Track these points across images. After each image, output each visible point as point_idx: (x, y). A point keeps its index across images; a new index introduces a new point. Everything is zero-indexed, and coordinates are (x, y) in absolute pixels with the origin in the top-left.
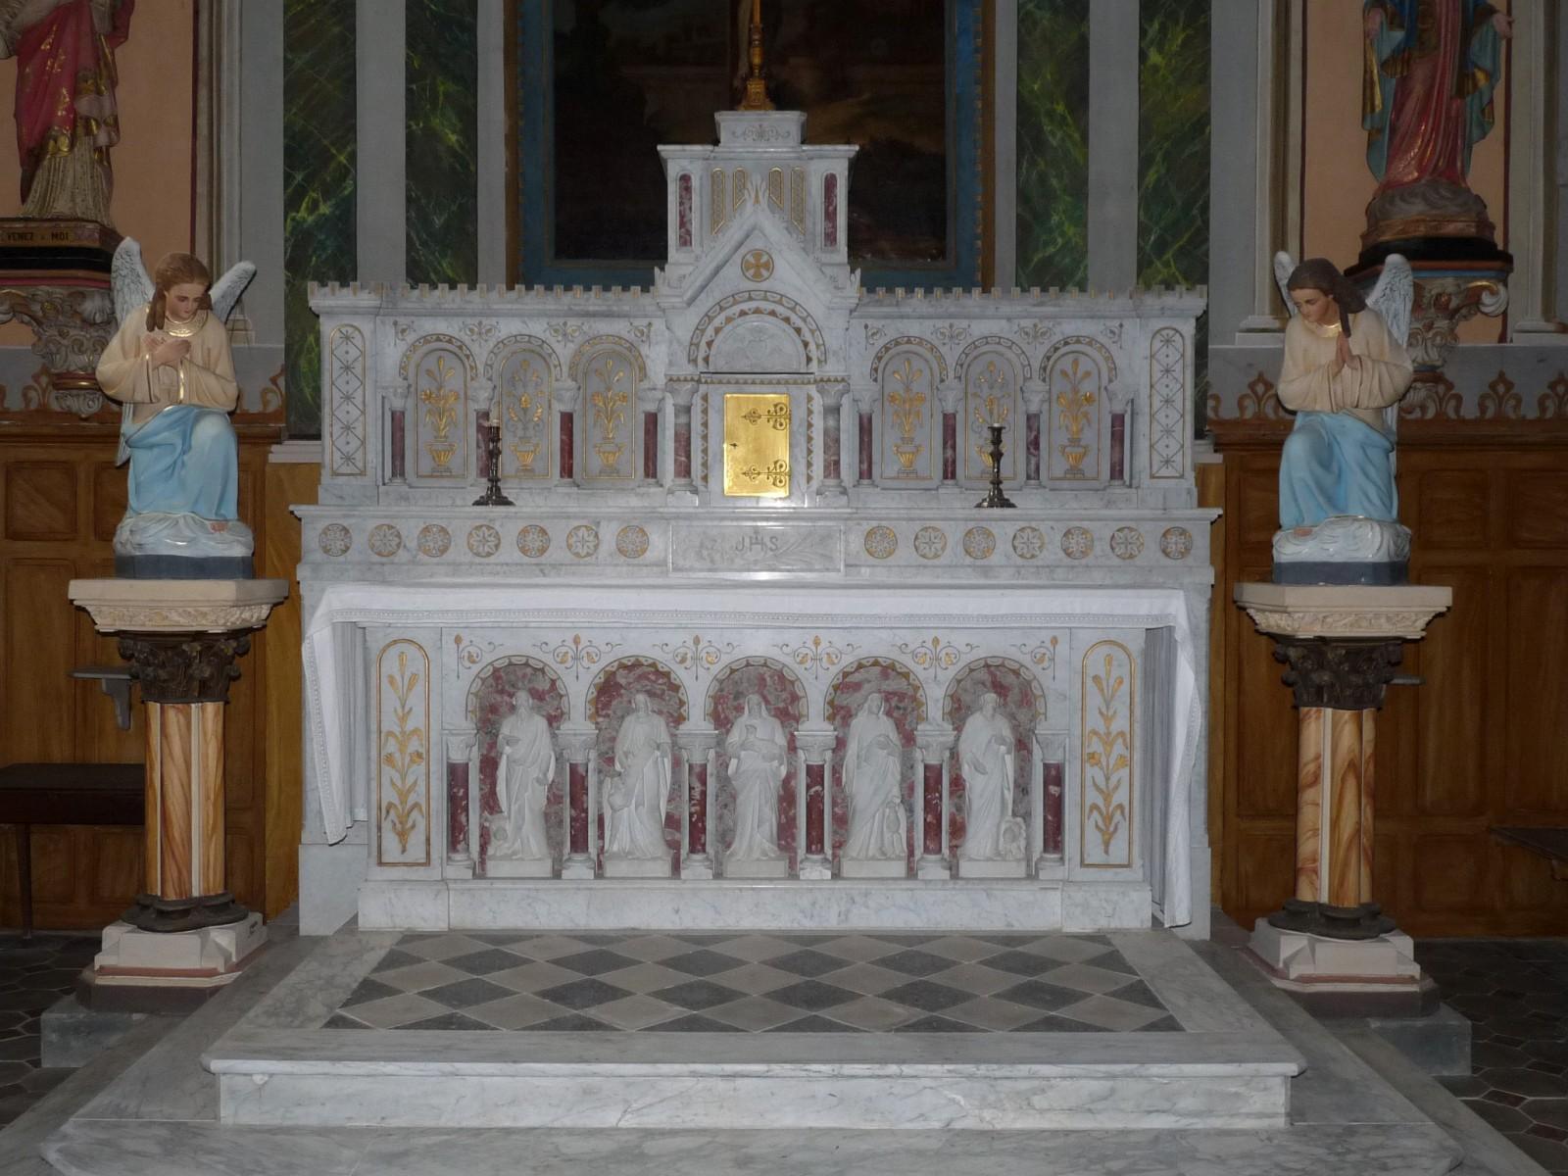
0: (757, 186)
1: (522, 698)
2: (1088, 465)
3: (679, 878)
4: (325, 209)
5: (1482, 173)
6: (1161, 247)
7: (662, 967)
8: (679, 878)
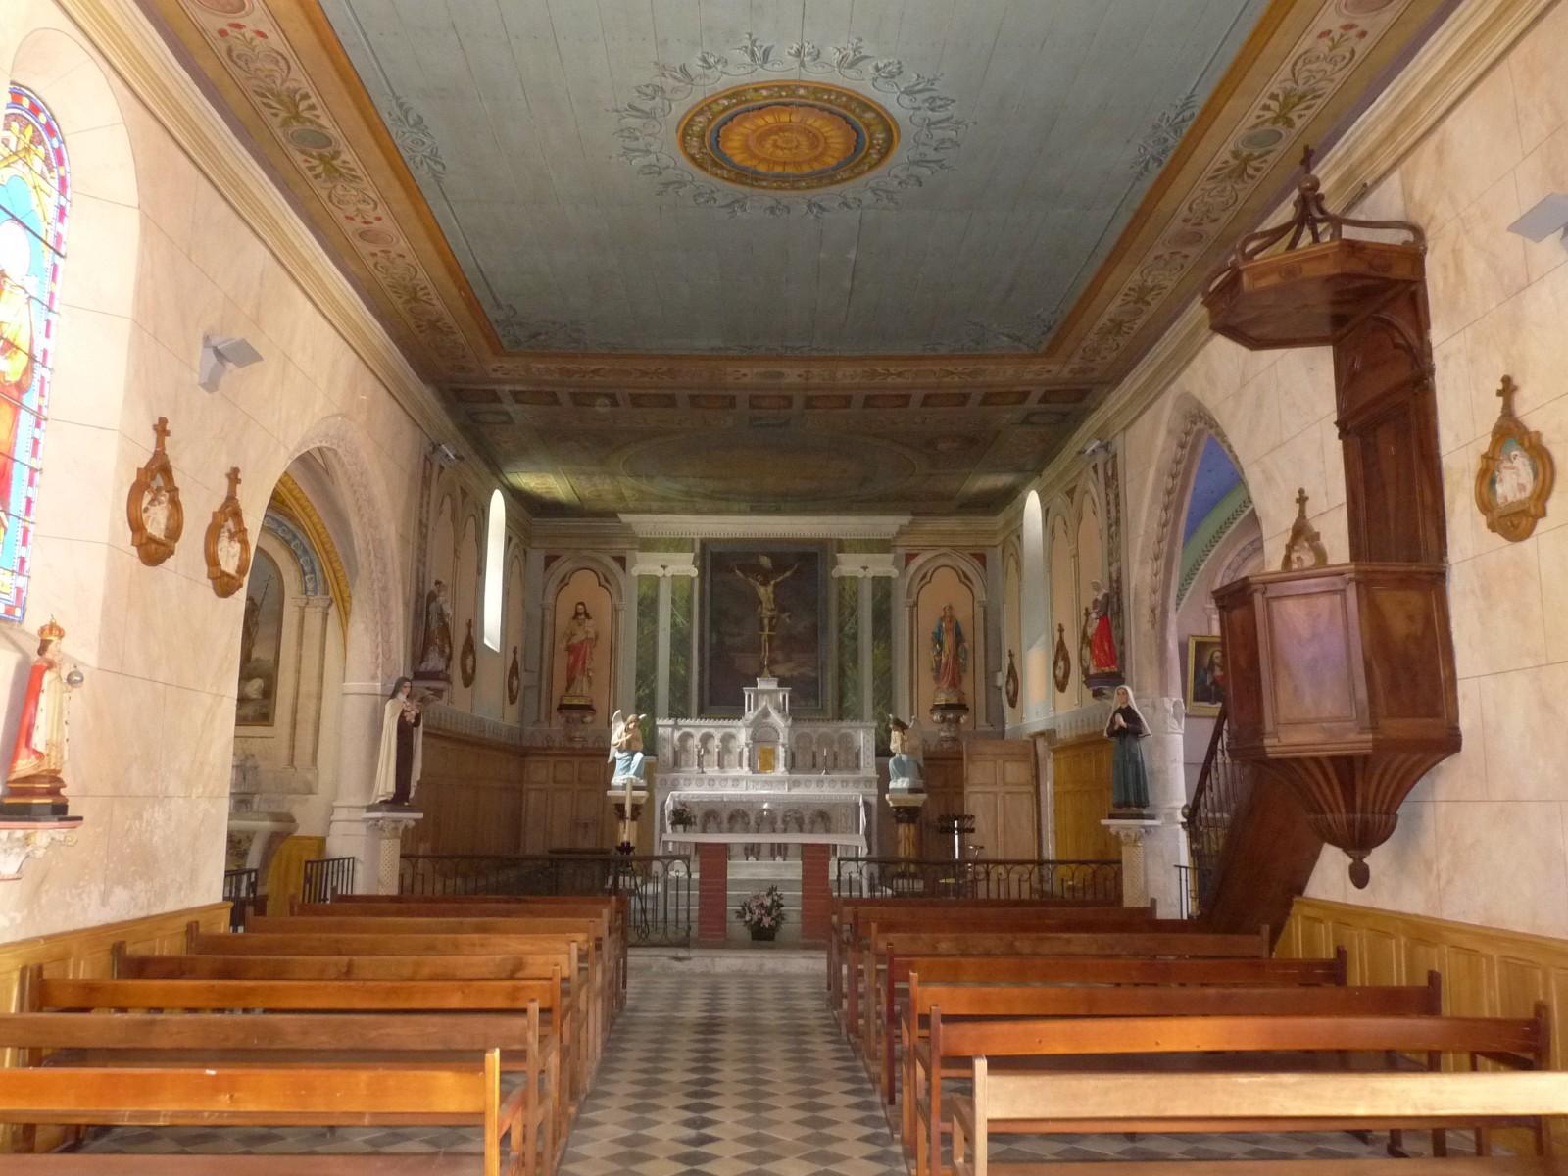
0: (766, 697)
1: (712, 819)
2: (850, 764)
3: (1392, 1132)
4: (647, 691)
5: (967, 686)
6: (878, 703)
7: (857, 1126)
8: (1392, 1132)
